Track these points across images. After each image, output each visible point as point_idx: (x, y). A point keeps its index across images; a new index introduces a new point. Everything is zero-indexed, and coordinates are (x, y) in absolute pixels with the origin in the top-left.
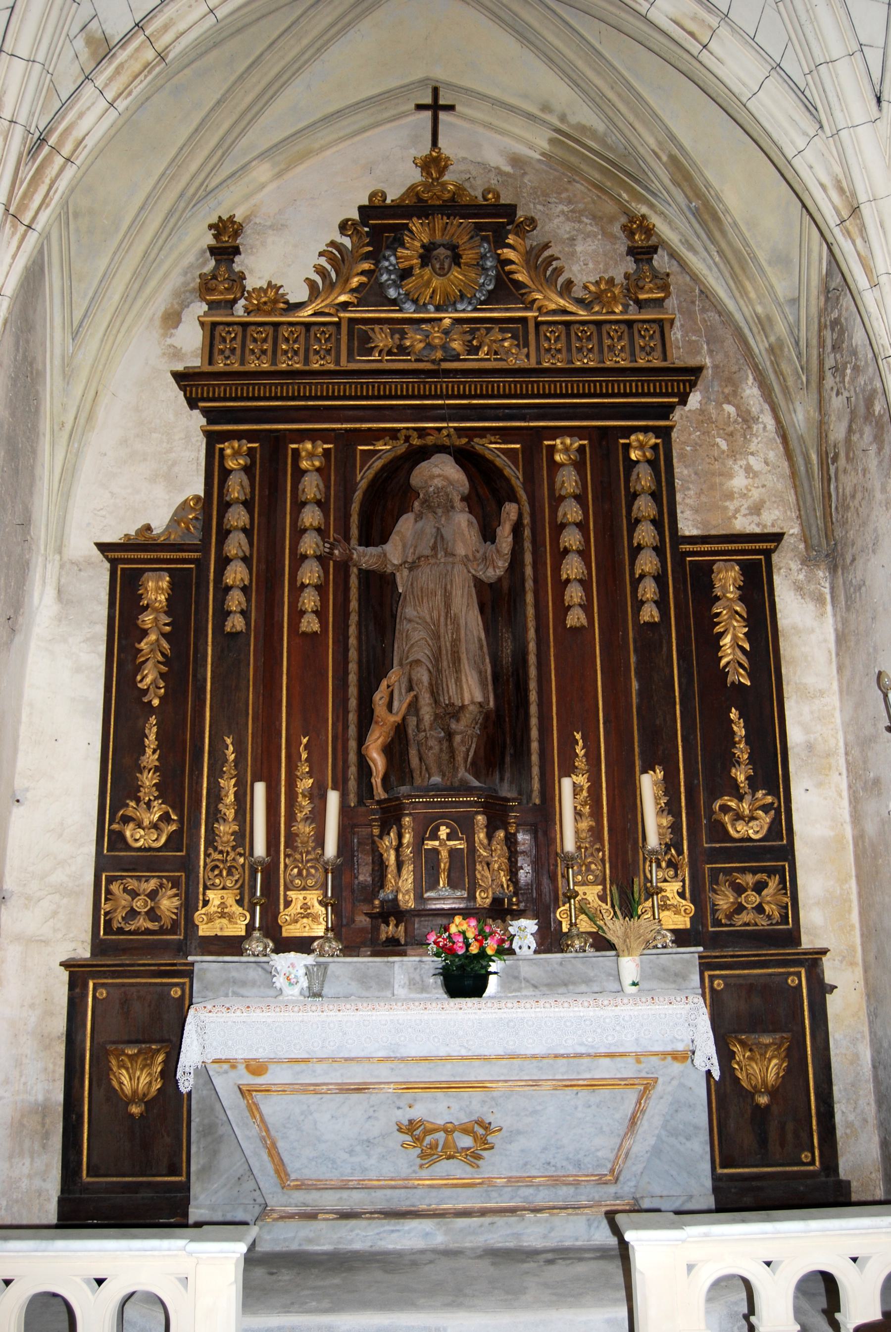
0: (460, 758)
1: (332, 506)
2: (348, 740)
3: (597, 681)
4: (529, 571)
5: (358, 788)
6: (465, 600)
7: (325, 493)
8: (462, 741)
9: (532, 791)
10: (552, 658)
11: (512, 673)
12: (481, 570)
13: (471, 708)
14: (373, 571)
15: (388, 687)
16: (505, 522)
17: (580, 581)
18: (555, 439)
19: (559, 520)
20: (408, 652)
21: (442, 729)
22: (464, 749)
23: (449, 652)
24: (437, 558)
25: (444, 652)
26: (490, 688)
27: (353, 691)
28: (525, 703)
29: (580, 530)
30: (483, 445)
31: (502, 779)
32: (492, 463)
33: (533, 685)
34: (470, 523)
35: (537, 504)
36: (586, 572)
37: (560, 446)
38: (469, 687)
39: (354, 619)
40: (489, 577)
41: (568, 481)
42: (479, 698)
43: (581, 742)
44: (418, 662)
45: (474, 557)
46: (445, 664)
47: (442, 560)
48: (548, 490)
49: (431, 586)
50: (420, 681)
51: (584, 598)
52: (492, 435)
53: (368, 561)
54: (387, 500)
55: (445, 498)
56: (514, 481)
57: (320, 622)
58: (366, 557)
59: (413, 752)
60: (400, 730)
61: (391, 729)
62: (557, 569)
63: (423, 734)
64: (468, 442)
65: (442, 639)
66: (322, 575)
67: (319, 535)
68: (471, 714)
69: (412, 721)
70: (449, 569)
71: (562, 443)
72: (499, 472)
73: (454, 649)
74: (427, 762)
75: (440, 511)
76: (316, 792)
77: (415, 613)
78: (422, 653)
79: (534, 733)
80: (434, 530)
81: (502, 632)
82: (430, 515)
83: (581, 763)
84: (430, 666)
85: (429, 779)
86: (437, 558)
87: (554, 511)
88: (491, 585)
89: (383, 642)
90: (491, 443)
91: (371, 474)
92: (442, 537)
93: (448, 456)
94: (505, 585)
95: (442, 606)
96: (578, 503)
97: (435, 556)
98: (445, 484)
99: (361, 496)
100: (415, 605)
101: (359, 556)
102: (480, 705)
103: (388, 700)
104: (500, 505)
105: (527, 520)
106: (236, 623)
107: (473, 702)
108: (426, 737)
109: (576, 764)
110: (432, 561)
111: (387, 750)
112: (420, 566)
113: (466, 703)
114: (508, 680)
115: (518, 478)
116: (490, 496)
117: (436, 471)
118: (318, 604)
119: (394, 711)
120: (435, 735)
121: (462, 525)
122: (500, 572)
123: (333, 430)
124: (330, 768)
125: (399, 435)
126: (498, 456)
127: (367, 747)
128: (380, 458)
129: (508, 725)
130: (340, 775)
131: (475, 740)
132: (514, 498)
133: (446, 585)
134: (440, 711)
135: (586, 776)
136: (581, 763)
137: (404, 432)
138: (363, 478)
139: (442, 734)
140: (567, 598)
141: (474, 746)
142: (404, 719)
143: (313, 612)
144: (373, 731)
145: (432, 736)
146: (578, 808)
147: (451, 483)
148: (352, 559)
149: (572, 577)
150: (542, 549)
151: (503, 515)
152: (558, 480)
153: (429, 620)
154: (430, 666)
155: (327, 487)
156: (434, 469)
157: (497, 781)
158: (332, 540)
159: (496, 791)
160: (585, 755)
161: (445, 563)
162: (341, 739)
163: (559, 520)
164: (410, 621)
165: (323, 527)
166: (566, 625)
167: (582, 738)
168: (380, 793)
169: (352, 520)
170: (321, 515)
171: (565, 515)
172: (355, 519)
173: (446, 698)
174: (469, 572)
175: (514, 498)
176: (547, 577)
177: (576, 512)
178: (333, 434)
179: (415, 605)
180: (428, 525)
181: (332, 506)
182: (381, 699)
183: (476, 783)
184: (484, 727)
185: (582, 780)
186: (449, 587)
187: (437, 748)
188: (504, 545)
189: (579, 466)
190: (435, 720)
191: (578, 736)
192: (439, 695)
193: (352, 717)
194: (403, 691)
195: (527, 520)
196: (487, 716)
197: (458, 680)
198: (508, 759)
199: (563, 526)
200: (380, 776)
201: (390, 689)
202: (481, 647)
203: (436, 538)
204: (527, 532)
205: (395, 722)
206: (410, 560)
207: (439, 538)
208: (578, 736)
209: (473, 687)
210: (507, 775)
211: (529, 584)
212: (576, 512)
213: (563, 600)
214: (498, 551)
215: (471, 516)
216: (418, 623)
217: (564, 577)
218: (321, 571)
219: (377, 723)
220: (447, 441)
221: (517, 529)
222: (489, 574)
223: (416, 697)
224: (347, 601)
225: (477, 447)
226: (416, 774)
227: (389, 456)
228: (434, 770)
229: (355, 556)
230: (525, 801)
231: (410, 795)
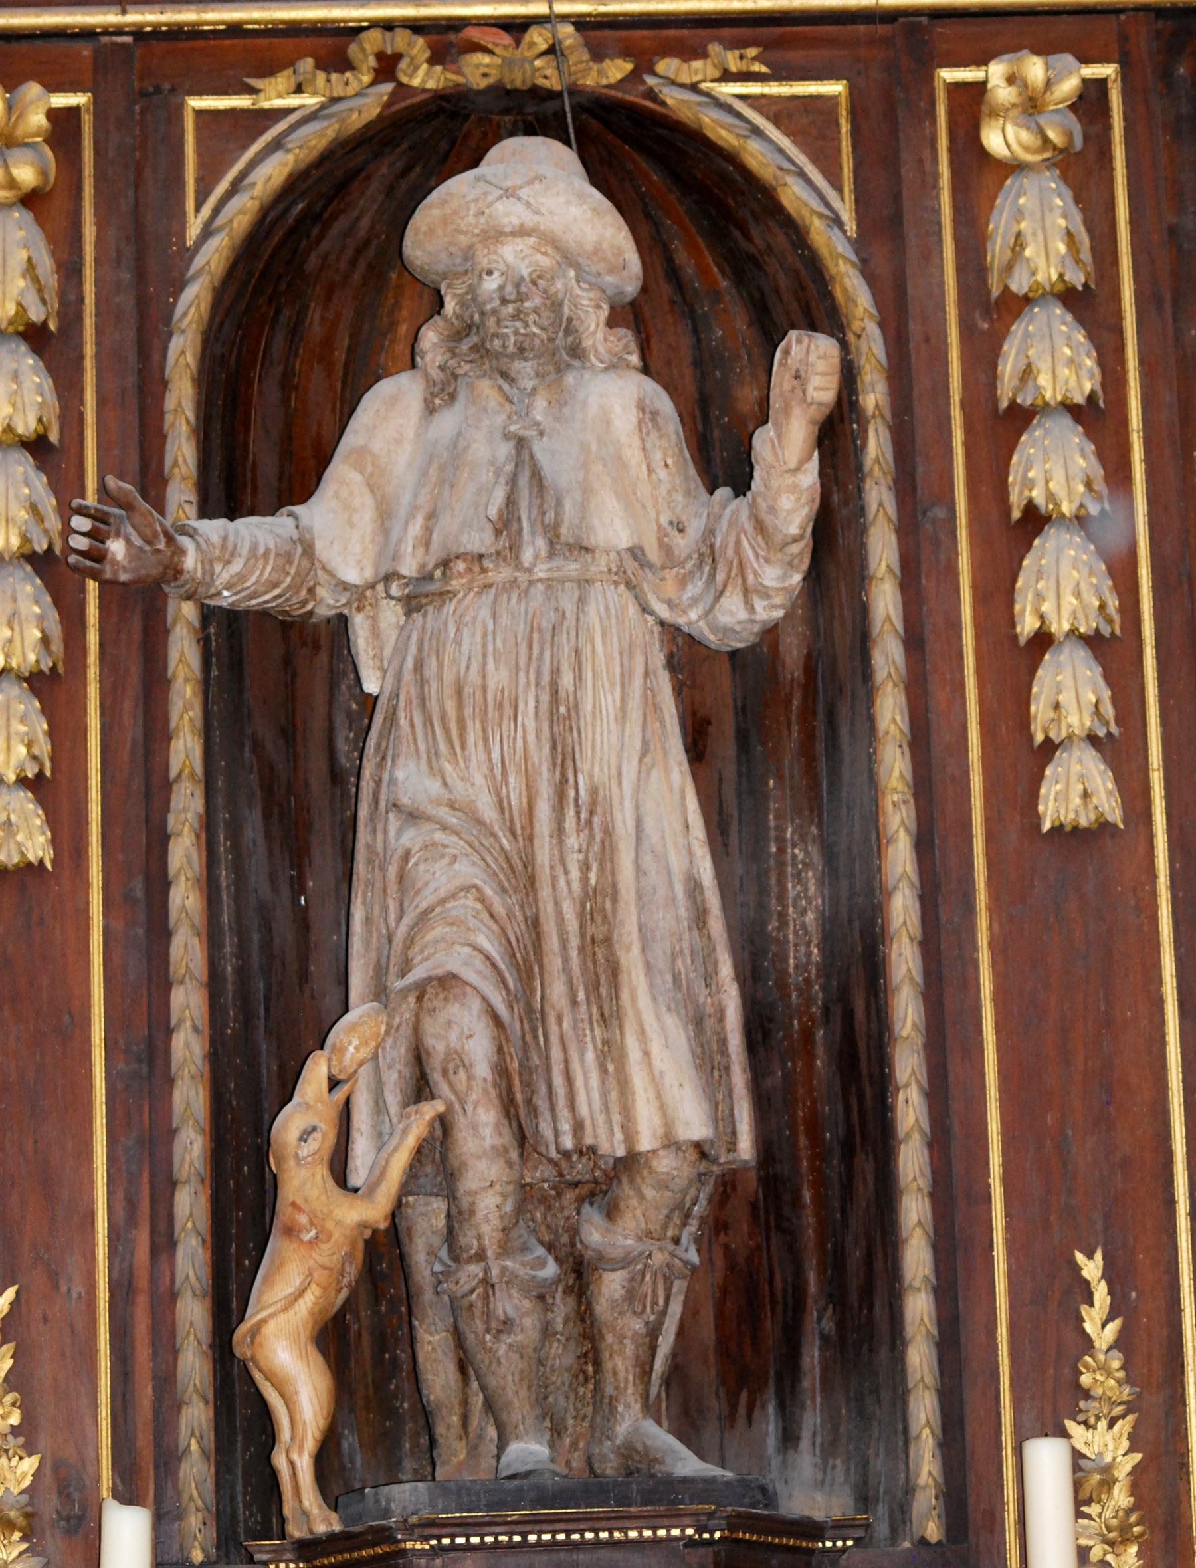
0: (620, 1364)
1: (89, 349)
2: (173, 1296)
3: (1163, 1043)
4: (885, 602)
5: (218, 1485)
6: (634, 729)
7: (62, 294)
8: (631, 1295)
9: (909, 1490)
10: (984, 957)
11: (826, 1009)
12: (695, 601)
13: (665, 1163)
14: (263, 615)
15: (333, 1084)
16: (787, 410)
17: (1094, 642)
18: (982, 61)
19: (1005, 393)
20: (410, 941)
21: (550, 1247)
22: (637, 1325)
23: (574, 942)
24: (518, 566)
25: (552, 942)
26: (739, 1079)
27: (190, 1098)
28: (873, 1132)
29: (1089, 434)
30: (694, 88)
31: (789, 1438)
32: (731, 158)
33: (908, 1066)
34: (647, 414)
35: (914, 327)
36: (1113, 603)
37: (1003, 93)
38: (656, 1081)
39: (186, 806)
40: (727, 631)
41: (1039, 233)
42: (694, 1124)
43: (1101, 1293)
44: (447, 982)
45: (667, 550)
46: (558, 991)
47: (540, 572)
48: (960, 269)
49: (498, 677)
50: (458, 1060)
51: (1109, 711)
52: (732, 44)
53: (242, 577)
54: (299, 329)
55: (547, 317)
56: (820, 235)
57: (52, 821)
58: (236, 558)
59: (433, 1343)
60: (383, 1257)
61: (350, 1256)
62: (998, 592)
63: (475, 1269)
64: (635, 77)
65: (545, 892)
66: (56, 631)
67: (41, 466)
68: (663, 1186)
69: (429, 1216)
70: (569, 605)
71: (1011, 80)
72: (765, 200)
73: (590, 930)
74: (492, 1382)
75: (525, 369)
76: (49, 1506)
77: (434, 787)
78: (464, 947)
79: (917, 1259)
80: (505, 450)
81: (781, 840)
82: (487, 388)
83: (1104, 1376)
84: (498, 1001)
85: (501, 1447)
86: (518, 566)
87: (983, 355)
88: (733, 654)
89: (299, 886)
90: (727, 76)
91: (241, 213)
92: (537, 476)
93: (557, 146)
94: (793, 651)
95: (541, 756)
96: (1081, 320)
97: (515, 548)
98: (545, 262)
99: (205, 306)
100: (433, 754)
101: (207, 562)
102: (701, 1149)
103: (331, 1139)
104: (771, 338)
105: (874, 396)
106: (1076, 791)
107: (671, 1143)
108: (486, 1282)
109: (1085, 1379)
110: (501, 574)
111: (332, 1338)
112: (450, 594)
113: (645, 1143)
114: (807, 1035)
115: (837, 222)
116: (724, 284)
117: (510, 213)
118: (44, 748)
119: (358, 1177)
120: (523, 1272)
121: (617, 415)
122: (768, 612)
123: (88, 34)
124: (105, 1412)
125: (353, 50)
126: (757, 131)
127: (255, 1331)
128: (277, 145)
129: (809, 1219)
130: (144, 1440)
131: (679, 1286)
132: (823, 314)
133: (556, 672)
134: (540, 1174)
135: (1124, 1426)
136: (1104, 1376)
137: (373, 40)
138: (214, 227)
139: (551, 1269)
140: (1039, 709)
141: (676, 1309)
142: (396, 1212)
143: (22, 781)
144: (279, 1266)
145: (510, 1279)
146: (1096, 1554)
147: (568, 258)
148: (179, 572)
149: (1060, 626)
150: (940, 513)
151: (781, 381)
152: (1000, 228)
153: (489, 813)
154: (498, 1001)
155: (70, 270)
156: (500, 207)
157: (772, 1442)
158: (91, 500)
159: (768, 1496)
160: (1119, 1344)
161: (549, 583)
162: (141, 1297)
163: (1005, 393)
164: (413, 816)
165: (54, 437)
166: (1037, 819)
167: (1109, 1274)
168: (309, 1511)
169: (170, 403)
170: (48, 383)
171: (1027, 373)
172: (181, 400)
173: (566, 1127)
174: (645, 609)
175: (823, 314)
176: (957, 626)
177: (1071, 361)
178: (86, 50)
179: (433, 754)
180: (479, 426)
181: (89, 349)
182: (304, 1137)
183: (687, 1463)
184: (717, 1226)
185: (1109, 1444)
186: (567, 680)
187: (529, 1326)
188: (786, 502)
189: (1082, 170)
190: (519, 1210)
191: (1091, 1268)
192: (534, 1111)
193: (190, 1205)
194: (393, 1100)
195: (874, 396)
196: (727, 1185)
197: (611, 1055)
198: (812, 1356)
199: (1020, 418)
200: (310, 1445)
201: (340, 1094)
202: (700, 918)
203: (513, 481)
204: (877, 446)
205: (363, 1225)
206: (409, 567)
207: (524, 480)
208: (1091, 1268)
209: (670, 1081)
210: (811, 1420)
211: (888, 656)
212: (1071, 361)
213: (1024, 721)
214: (761, 527)
215: (650, 386)
216: (444, 827)
217: (1027, 626)
218: (54, 615)
219: (290, 1231)
220: (549, 77)
221: (836, 436)
222: (724, 619)
223: (444, 1124)
224: (156, 732)
225: (673, 97)
226: (447, 1426)
227: (313, 140)
228: (519, 1408)
229: (190, 562)
230: (882, 1529)
231: (432, 1524)
